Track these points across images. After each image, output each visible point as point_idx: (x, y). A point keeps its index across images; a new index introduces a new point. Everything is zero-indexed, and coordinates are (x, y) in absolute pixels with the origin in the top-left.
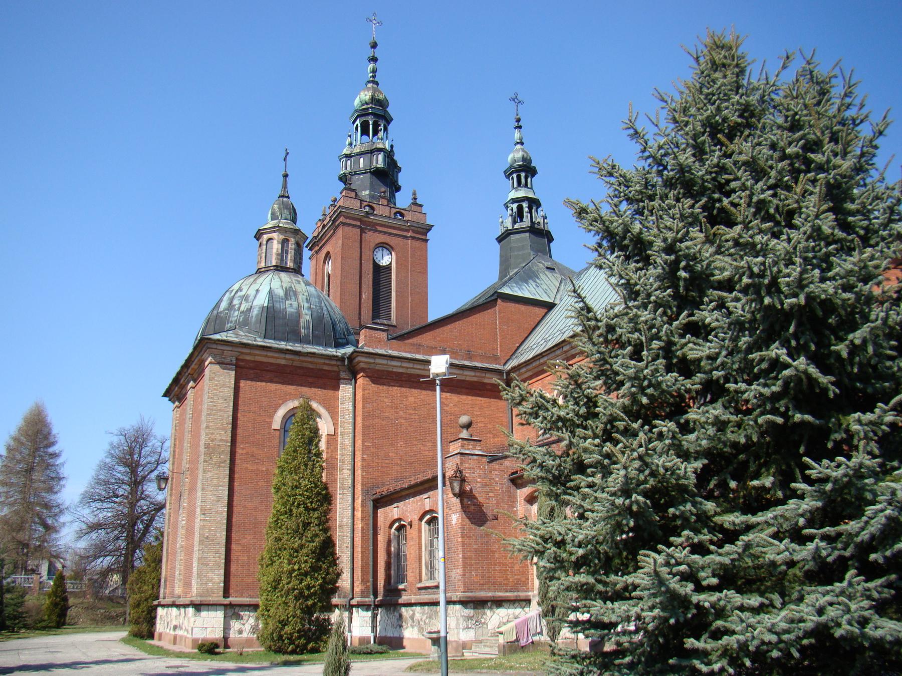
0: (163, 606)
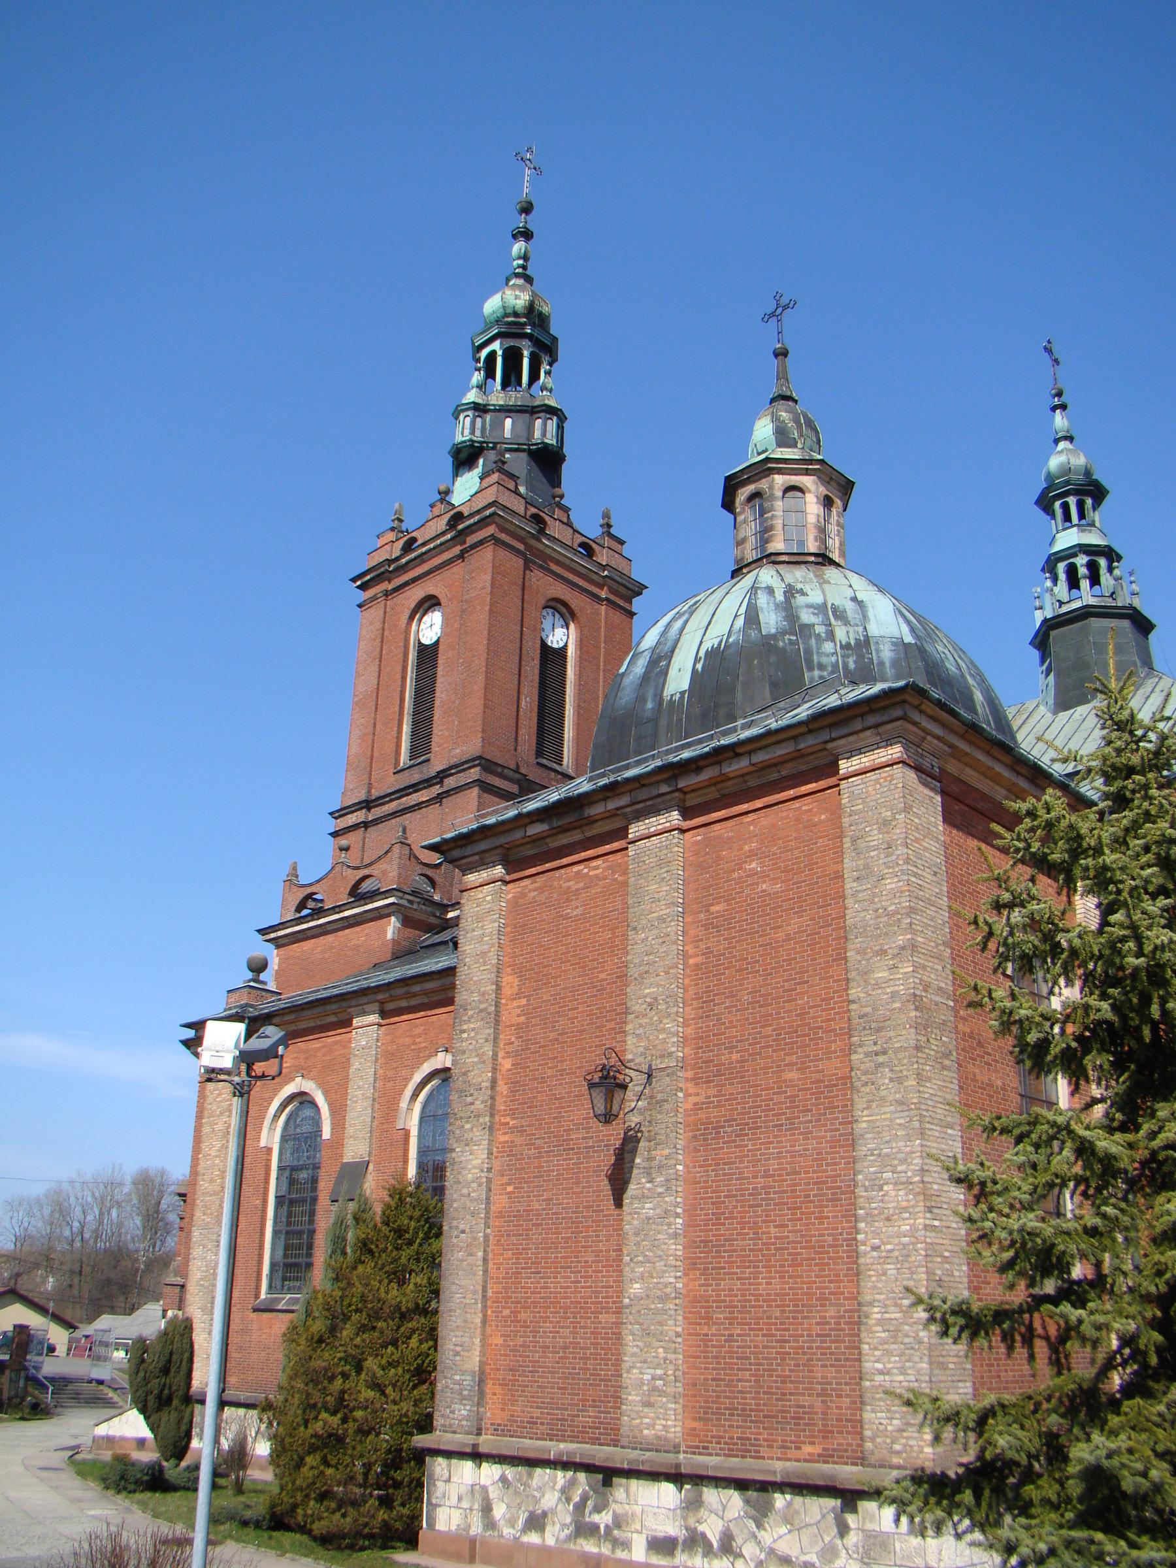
0: (449, 1454)
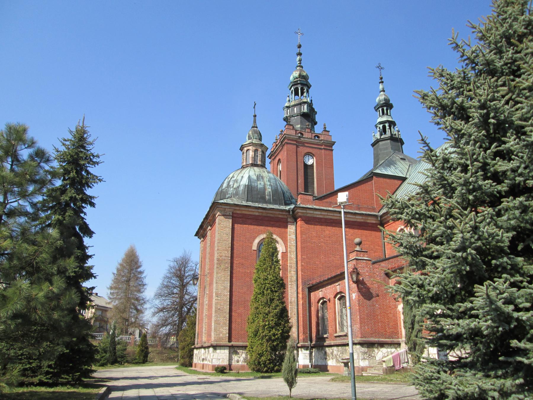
0: (197, 348)
